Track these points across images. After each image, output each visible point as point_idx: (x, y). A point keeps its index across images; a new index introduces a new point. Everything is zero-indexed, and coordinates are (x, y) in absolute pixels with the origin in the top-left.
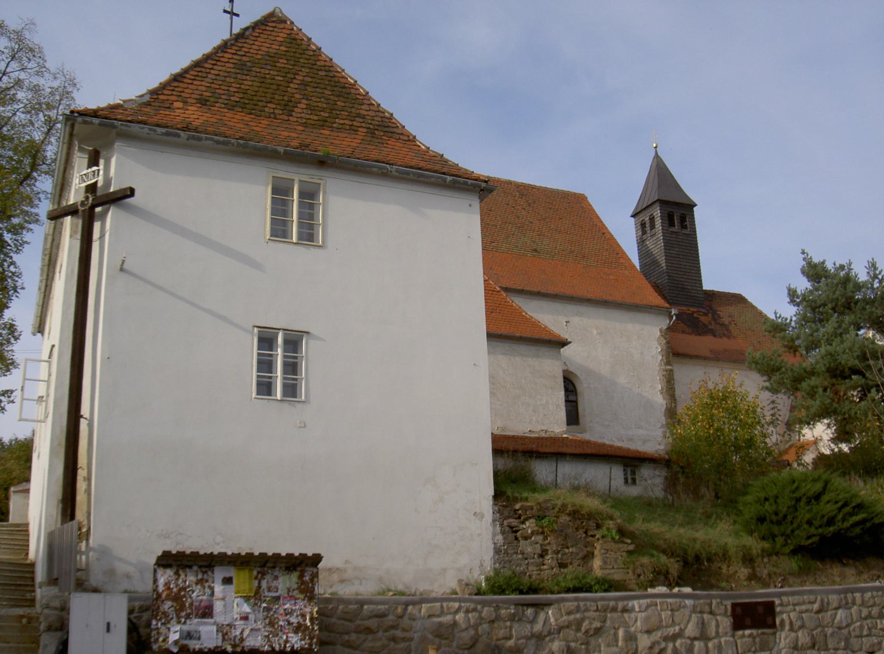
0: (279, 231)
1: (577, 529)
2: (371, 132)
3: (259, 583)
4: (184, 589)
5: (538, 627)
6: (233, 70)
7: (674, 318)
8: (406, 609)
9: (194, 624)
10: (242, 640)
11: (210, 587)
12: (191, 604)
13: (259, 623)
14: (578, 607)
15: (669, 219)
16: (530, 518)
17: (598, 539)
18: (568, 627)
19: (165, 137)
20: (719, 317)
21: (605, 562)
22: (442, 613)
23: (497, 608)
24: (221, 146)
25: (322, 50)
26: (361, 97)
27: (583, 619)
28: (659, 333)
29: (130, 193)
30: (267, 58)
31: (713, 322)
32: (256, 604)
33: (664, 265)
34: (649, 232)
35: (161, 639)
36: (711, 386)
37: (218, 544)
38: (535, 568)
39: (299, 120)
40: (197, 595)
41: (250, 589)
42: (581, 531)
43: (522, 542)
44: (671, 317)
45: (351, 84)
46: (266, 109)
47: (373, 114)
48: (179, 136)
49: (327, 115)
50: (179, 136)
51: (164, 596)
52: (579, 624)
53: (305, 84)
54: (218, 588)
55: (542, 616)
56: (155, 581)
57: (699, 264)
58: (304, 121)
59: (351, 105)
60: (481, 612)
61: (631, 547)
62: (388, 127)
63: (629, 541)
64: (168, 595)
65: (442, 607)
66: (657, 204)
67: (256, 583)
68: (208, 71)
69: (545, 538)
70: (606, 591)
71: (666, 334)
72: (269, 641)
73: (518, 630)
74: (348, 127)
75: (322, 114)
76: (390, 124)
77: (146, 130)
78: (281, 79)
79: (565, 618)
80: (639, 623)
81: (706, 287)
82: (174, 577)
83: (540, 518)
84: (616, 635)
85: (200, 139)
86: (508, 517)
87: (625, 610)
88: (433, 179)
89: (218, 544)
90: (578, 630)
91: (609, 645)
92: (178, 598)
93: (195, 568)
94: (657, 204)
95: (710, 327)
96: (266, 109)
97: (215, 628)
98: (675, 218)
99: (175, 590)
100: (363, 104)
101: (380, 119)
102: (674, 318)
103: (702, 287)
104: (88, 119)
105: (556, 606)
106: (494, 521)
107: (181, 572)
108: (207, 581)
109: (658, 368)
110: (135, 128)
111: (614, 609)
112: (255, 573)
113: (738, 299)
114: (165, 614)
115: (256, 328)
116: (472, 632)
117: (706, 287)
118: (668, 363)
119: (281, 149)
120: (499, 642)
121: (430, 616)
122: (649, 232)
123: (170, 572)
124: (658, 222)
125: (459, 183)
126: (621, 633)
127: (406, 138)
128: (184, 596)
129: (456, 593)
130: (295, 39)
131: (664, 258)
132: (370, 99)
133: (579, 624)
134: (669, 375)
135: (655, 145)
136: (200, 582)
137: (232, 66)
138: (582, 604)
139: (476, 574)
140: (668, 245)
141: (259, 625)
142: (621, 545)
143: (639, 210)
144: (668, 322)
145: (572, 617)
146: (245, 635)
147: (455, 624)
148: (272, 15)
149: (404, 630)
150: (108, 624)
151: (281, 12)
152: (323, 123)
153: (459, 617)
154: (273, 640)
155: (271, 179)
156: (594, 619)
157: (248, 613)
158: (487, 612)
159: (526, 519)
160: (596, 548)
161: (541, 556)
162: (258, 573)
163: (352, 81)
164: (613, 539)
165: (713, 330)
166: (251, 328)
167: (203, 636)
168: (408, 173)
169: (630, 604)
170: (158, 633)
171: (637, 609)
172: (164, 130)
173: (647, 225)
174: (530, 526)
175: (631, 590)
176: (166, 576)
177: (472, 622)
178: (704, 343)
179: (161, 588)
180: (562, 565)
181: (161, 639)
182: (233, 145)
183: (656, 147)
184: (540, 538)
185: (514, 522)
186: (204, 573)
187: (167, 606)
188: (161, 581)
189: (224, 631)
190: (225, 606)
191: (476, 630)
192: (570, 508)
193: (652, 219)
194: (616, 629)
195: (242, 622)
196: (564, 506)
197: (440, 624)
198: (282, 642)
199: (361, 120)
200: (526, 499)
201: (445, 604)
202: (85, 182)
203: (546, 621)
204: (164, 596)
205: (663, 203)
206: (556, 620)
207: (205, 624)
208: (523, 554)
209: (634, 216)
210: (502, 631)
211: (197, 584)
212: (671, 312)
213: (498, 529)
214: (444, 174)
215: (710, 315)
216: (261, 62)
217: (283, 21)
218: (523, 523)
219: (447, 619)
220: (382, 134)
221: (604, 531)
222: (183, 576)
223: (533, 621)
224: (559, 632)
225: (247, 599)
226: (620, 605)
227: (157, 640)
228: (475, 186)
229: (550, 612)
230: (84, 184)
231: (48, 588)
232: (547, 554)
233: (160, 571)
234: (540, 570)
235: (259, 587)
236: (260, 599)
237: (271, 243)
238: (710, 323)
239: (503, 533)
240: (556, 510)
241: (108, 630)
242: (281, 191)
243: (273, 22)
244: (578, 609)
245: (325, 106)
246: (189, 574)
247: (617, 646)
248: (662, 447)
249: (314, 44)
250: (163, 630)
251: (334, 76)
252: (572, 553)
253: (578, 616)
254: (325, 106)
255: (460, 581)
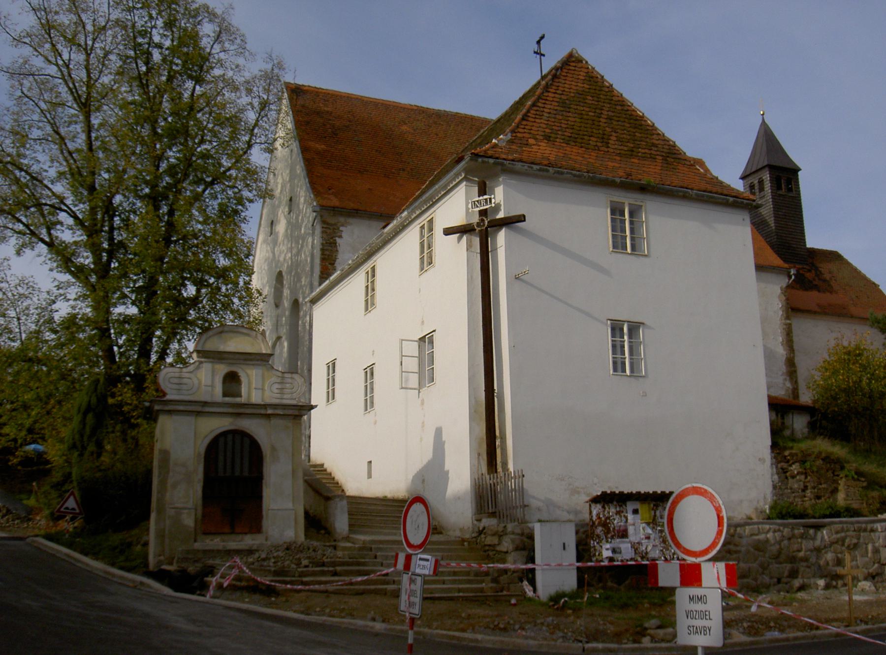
0: (618, 244)
1: (827, 471)
2: (665, 159)
3: (655, 513)
4: (608, 518)
5: (818, 543)
6: (558, 108)
7: (793, 277)
8: (736, 530)
9: (617, 542)
10: (647, 553)
11: (624, 516)
12: (614, 529)
13: (657, 541)
14: (843, 528)
15: (777, 183)
16: (796, 462)
17: (842, 478)
18: (837, 542)
19: (538, 172)
20: (820, 272)
21: (847, 496)
22: (759, 533)
23: (793, 529)
24: (575, 178)
25: (614, 86)
26: (650, 128)
27: (846, 537)
28: (779, 291)
29: (521, 218)
30: (577, 95)
31: (816, 278)
32: (654, 528)
33: (773, 225)
34: (758, 194)
35: (597, 554)
36: (846, 344)
37: (596, 484)
38: (800, 500)
39: (615, 151)
40: (617, 522)
41: (650, 517)
42: (830, 472)
43: (790, 480)
44: (790, 277)
45: (640, 117)
46: (591, 142)
47: (662, 143)
48: (547, 171)
49: (632, 145)
50: (547, 171)
51: (597, 523)
52: (843, 540)
53: (610, 118)
54: (630, 517)
55: (819, 534)
56: (591, 513)
57: (803, 224)
58: (618, 152)
59: (646, 136)
60: (783, 532)
61: (865, 484)
62: (675, 154)
63: (863, 479)
64: (599, 523)
65: (759, 528)
66: (767, 169)
67: (653, 513)
68: (542, 109)
69: (806, 477)
70: (851, 516)
71: (785, 292)
72: (663, 553)
73: (807, 545)
74: (649, 156)
75: (628, 144)
76: (676, 152)
77: (526, 167)
78: (593, 114)
79: (834, 536)
80: (881, 540)
81: (808, 246)
82: (602, 510)
83: (803, 462)
84: (866, 548)
85: (562, 173)
86: (781, 462)
87: (872, 531)
88: (720, 201)
89: (596, 484)
90: (843, 545)
91: (862, 556)
92: (605, 525)
93: (615, 503)
94: (767, 169)
95: (815, 283)
96: (591, 142)
97: (629, 545)
98: (783, 181)
99: (603, 519)
100: (653, 134)
101: (667, 147)
102: (793, 277)
103: (805, 245)
104: (486, 160)
105: (828, 527)
106: (772, 464)
107: (606, 507)
108: (623, 512)
109: (779, 322)
110: (519, 166)
111: (865, 530)
112: (652, 505)
113: (834, 256)
114: (598, 536)
115: (609, 322)
116: (778, 547)
117: (808, 246)
118: (788, 318)
119: (618, 180)
120: (794, 554)
121: (752, 535)
122: (758, 194)
123: (599, 506)
124: (767, 186)
125: (737, 202)
126: (870, 547)
127: (689, 163)
128: (609, 523)
129: (751, 519)
130: (592, 77)
131: (773, 219)
132: (656, 129)
133: (843, 540)
134: (789, 328)
135: (762, 113)
136: (618, 513)
137: (557, 104)
138: (845, 526)
139: (761, 504)
140: (777, 207)
141: (657, 542)
142: (858, 483)
143: (748, 173)
144: (787, 281)
145: (839, 536)
146: (649, 550)
147: (767, 541)
148: (571, 55)
149: (735, 545)
150: (564, 544)
151: (577, 52)
152: (631, 153)
153: (770, 535)
154: (665, 553)
155: (609, 202)
156: (853, 537)
157: (650, 534)
158: (786, 531)
159: (793, 463)
160: (840, 484)
161: (803, 491)
162: (654, 505)
163: (641, 114)
164: (853, 478)
165: (816, 285)
166: (605, 321)
167: (623, 551)
168: (703, 196)
169: (875, 527)
170: (595, 550)
171: (880, 530)
172: (538, 167)
173: (757, 187)
174: (795, 468)
175: (866, 516)
176: (597, 509)
177: (778, 538)
178: (811, 298)
179: (594, 518)
180: (818, 497)
181: (597, 554)
182: (585, 177)
183: (763, 115)
184: (803, 477)
185: (785, 465)
186: (620, 506)
187: (599, 530)
188: (594, 513)
189: (635, 547)
190: (635, 530)
191: (780, 544)
192: (823, 455)
193: (761, 182)
194: (867, 544)
195: (646, 541)
196: (820, 453)
197: (759, 541)
198: (671, 554)
199: (656, 149)
200: (792, 448)
201: (760, 526)
202: (477, 207)
203: (823, 538)
204: (597, 523)
205: (771, 168)
206: (829, 537)
207: (623, 542)
208: (791, 489)
209: (743, 178)
210: (796, 546)
211: (616, 514)
212: (790, 272)
213: (775, 470)
214: (726, 195)
215: (813, 271)
216: (575, 99)
217: (580, 60)
218: (791, 466)
219: (762, 537)
220: (672, 160)
221: (845, 472)
222: (607, 509)
223: (814, 539)
224: (830, 547)
225: (648, 524)
226: (869, 526)
227: (595, 555)
228: (747, 205)
229: (825, 532)
230: (478, 209)
231: (489, 519)
232: (807, 489)
233: (593, 506)
234: (803, 501)
235: (655, 516)
236: (656, 524)
237: (613, 254)
238: (814, 280)
239: (778, 473)
240: (813, 456)
241: (564, 548)
242: (616, 211)
243: (573, 62)
244: (842, 530)
245: (629, 137)
246: (611, 507)
247: (867, 556)
248: (783, 393)
249: (607, 82)
250: (597, 547)
251: (628, 110)
252: (824, 488)
253: (843, 534)
254: (629, 137)
255: (756, 509)
